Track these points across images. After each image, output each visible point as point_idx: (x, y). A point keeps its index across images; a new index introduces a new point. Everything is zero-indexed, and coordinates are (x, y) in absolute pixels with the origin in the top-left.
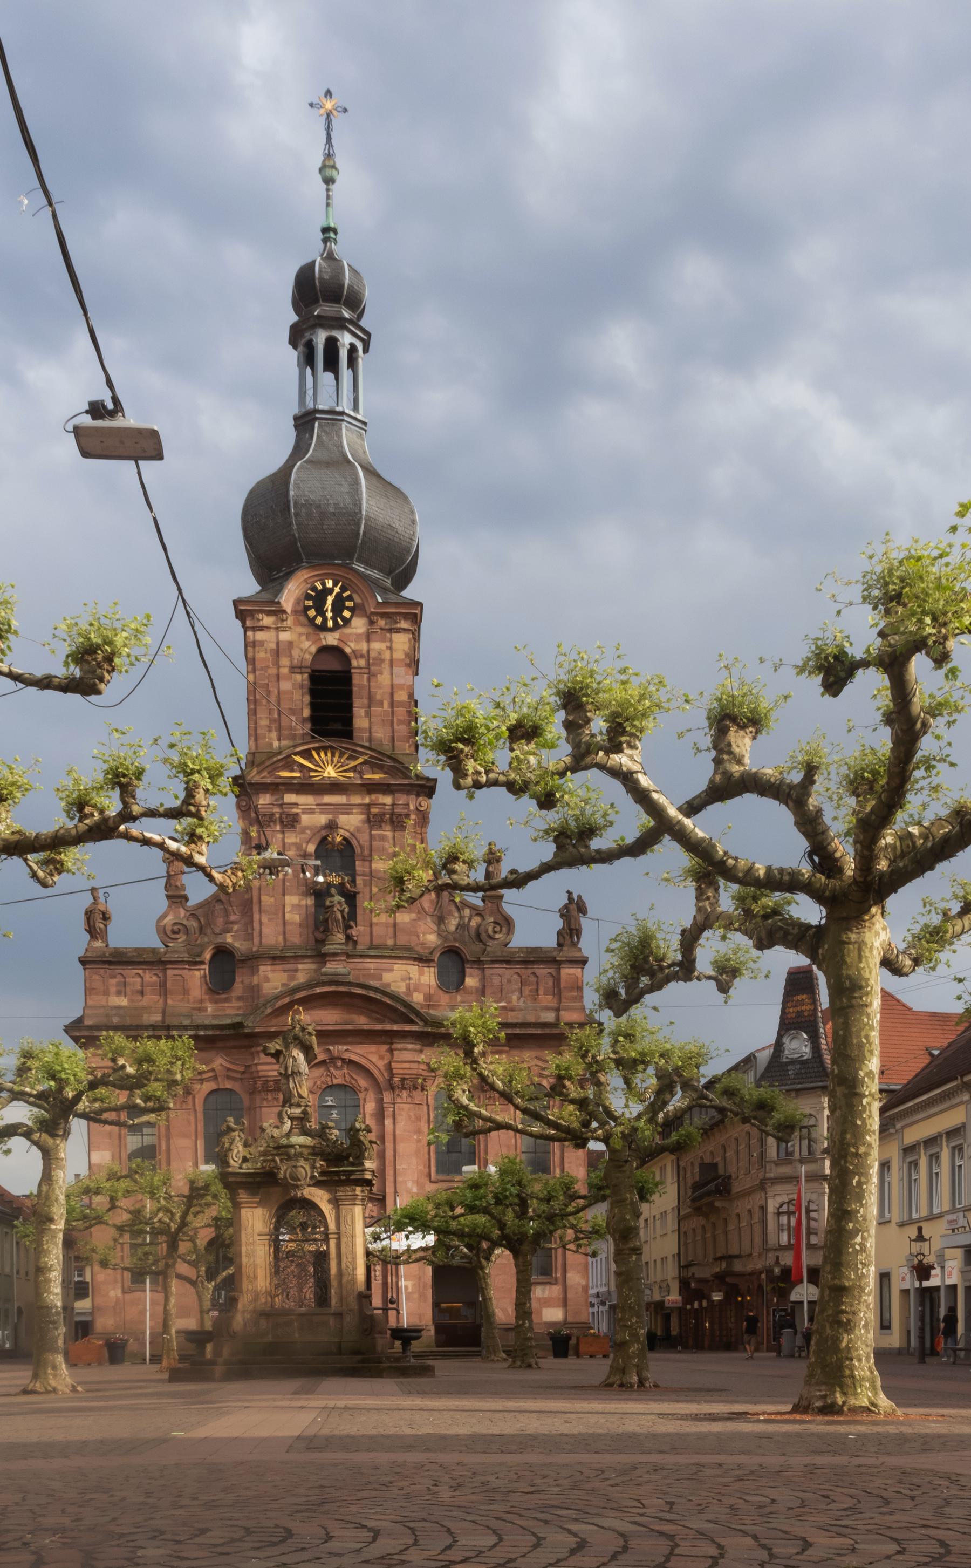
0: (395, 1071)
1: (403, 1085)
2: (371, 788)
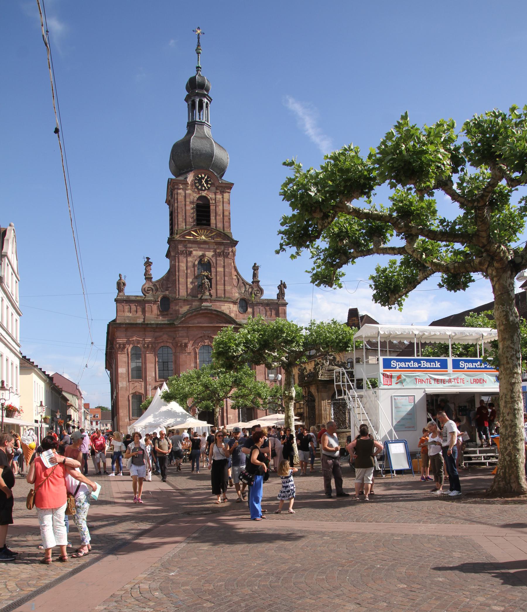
2: (217, 243)
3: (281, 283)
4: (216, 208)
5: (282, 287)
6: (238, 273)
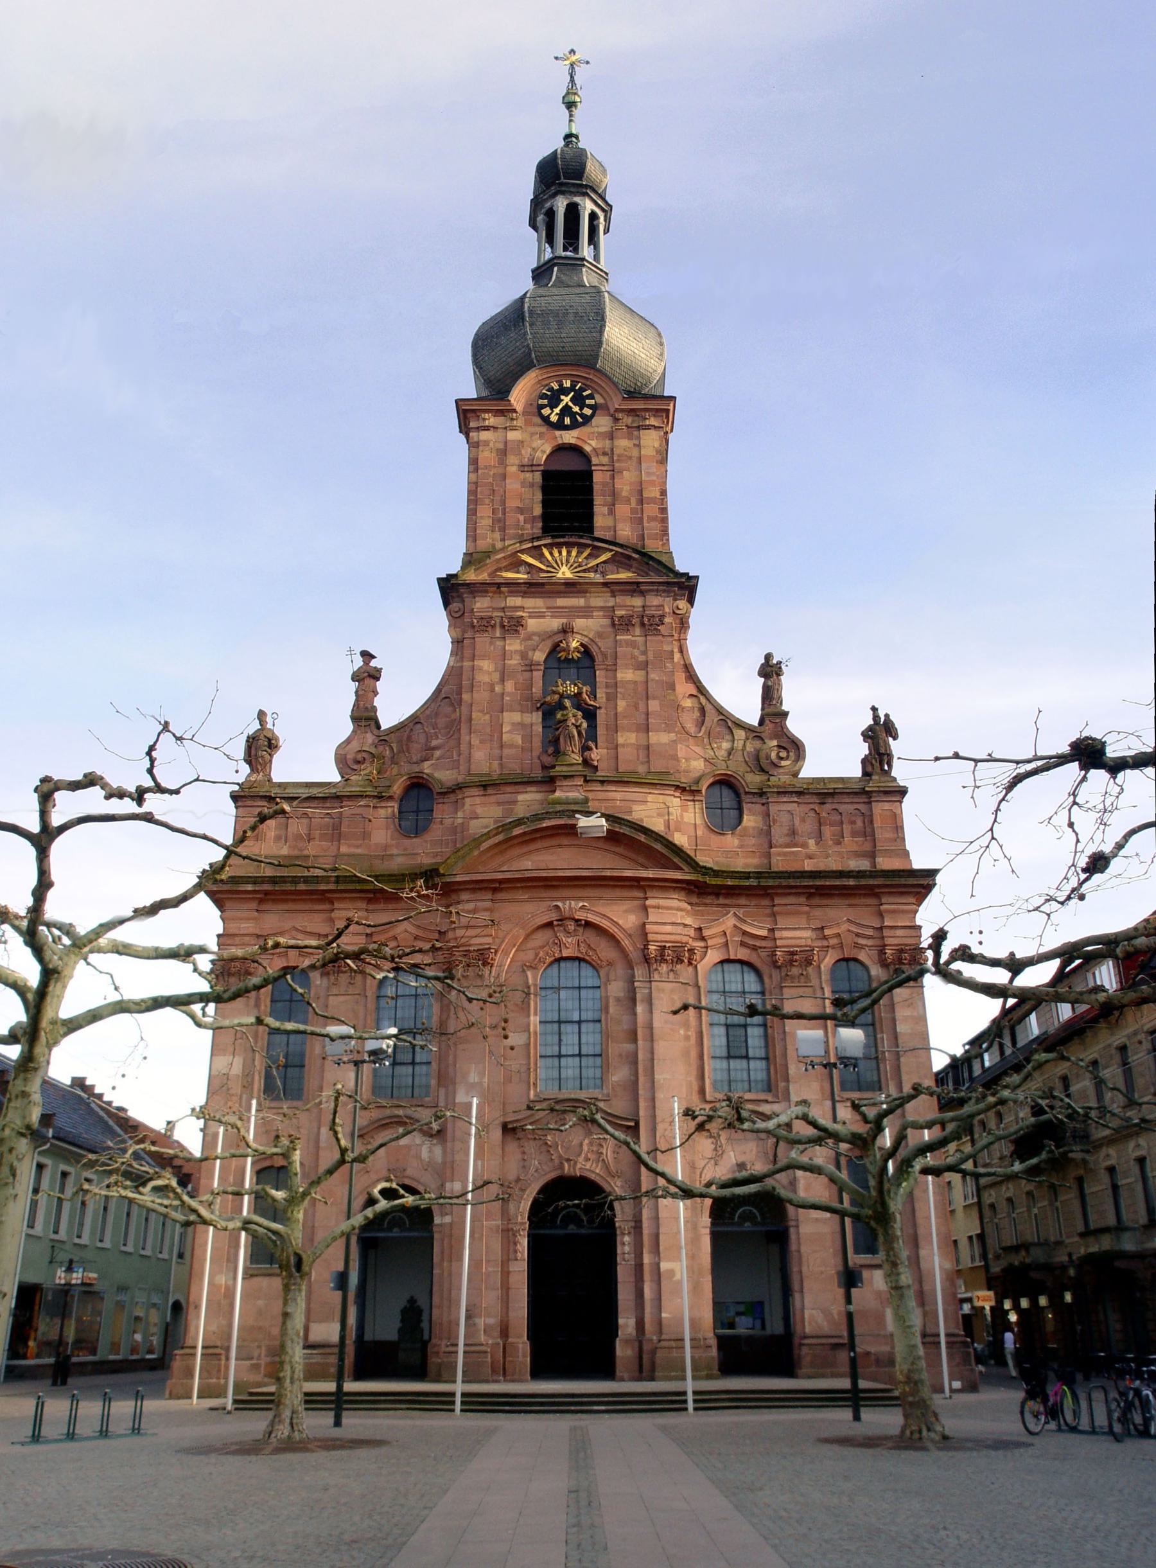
0: (650, 937)
1: (662, 955)
3: (876, 717)
4: (613, 477)
5: (880, 733)
6: (701, 690)
